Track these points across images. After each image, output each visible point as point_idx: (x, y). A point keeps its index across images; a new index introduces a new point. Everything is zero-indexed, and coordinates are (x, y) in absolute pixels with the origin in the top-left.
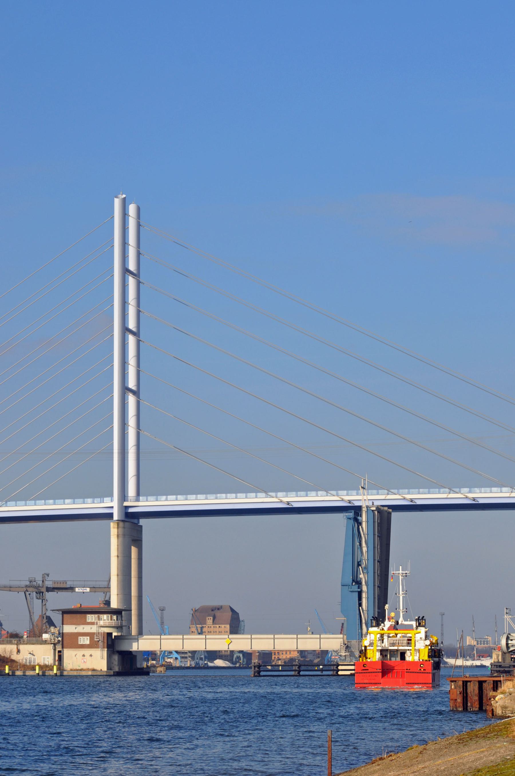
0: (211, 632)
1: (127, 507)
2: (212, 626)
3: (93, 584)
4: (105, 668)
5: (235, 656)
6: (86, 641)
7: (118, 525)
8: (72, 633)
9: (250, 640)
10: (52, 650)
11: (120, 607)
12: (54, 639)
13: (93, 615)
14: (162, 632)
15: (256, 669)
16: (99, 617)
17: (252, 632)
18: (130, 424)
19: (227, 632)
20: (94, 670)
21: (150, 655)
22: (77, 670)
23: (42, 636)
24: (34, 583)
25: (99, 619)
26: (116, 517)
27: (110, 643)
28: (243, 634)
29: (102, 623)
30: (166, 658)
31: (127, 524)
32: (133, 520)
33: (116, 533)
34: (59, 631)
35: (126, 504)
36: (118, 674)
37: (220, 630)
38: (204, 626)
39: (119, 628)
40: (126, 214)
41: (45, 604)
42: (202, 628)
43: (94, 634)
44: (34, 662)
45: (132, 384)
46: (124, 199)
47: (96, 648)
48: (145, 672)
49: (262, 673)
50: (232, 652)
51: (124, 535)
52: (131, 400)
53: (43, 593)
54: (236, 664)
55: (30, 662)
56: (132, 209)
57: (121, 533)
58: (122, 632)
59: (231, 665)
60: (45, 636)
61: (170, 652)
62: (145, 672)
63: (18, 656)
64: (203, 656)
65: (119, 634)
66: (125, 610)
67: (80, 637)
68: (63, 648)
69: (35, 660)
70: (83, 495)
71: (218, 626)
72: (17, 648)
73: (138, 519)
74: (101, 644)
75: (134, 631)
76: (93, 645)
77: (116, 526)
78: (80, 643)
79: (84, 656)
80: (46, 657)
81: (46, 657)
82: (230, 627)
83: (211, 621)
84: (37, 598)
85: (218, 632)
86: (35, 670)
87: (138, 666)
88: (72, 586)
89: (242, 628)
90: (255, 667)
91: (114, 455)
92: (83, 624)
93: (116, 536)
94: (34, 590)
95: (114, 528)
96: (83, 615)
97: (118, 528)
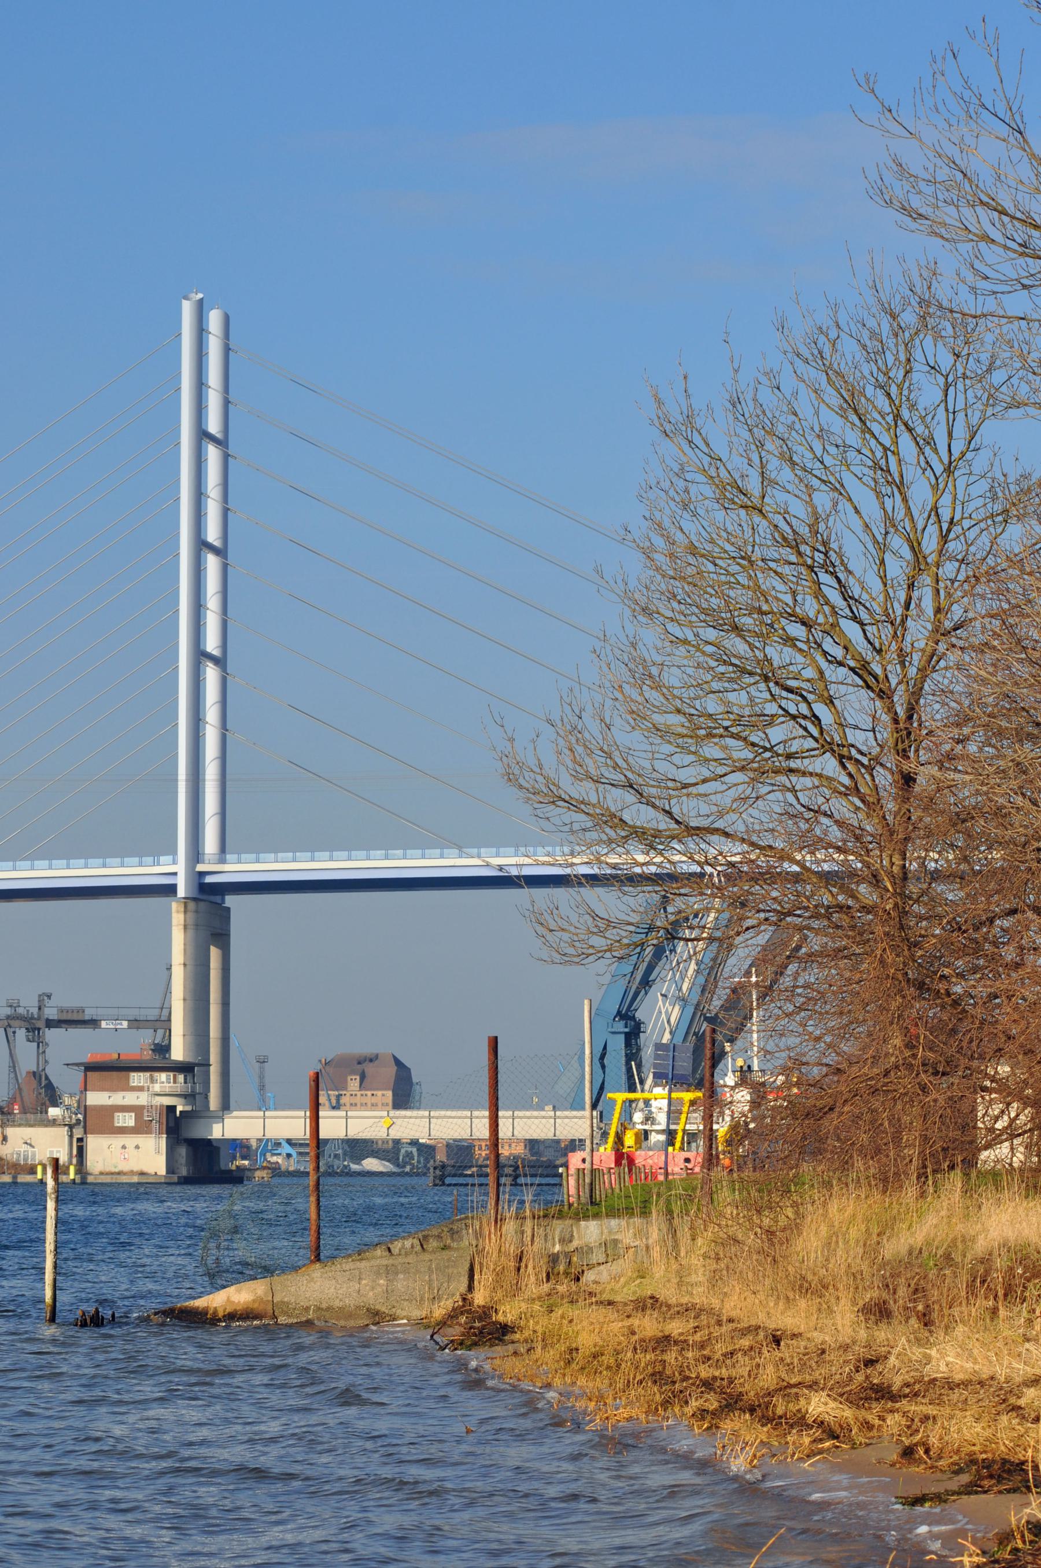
0: (356, 1105)
1: (202, 874)
2: (359, 1093)
3: (134, 1013)
4: (162, 1171)
5: (403, 1151)
6: (127, 1120)
7: (186, 907)
8: (102, 1106)
9: (552, 1121)
10: (67, 1138)
11: (190, 1059)
12: (70, 1117)
13: (141, 1074)
14: (262, 1104)
15: (438, 1172)
16: (152, 1077)
17: (431, 1107)
18: (207, 719)
19: (387, 1105)
20: (142, 1174)
21: (240, 1146)
22: (112, 1174)
23: (47, 1112)
24: (20, 1010)
25: (153, 1081)
26: (181, 892)
27: (172, 1124)
28: (419, 1109)
29: (157, 1088)
30: (268, 1155)
31: (202, 904)
32: (213, 898)
33: (182, 922)
34: (79, 1102)
35: (200, 868)
36: (186, 1181)
37: (374, 1100)
38: (343, 1093)
39: (186, 1097)
40: (203, 330)
41: (44, 1052)
42: (339, 1097)
43: (142, 1107)
44: (33, 1159)
45: (212, 644)
46: (201, 302)
47: (147, 1133)
48: (236, 1178)
49: (448, 1180)
50: (397, 1142)
51: (197, 925)
52: (211, 674)
53: (39, 1029)
54: (404, 1167)
55: (26, 1159)
56: (214, 320)
57: (190, 921)
58: (193, 1104)
59: (395, 1169)
60: (53, 1112)
61: (278, 1144)
62: (236, 1178)
63: (4, 1147)
64: (340, 1152)
65: (189, 1108)
66: (199, 1065)
67: (116, 1114)
68: (85, 1133)
69: (34, 1154)
70: (122, 851)
71: (369, 1093)
72: (2, 1133)
73: (223, 895)
74: (155, 1125)
75: (214, 1101)
76: (141, 1128)
77: (183, 909)
78: (117, 1125)
79: (124, 1147)
80: (55, 1150)
81: (55, 1150)
82: (394, 1095)
83: (357, 1084)
84: (29, 1040)
85: (369, 1105)
86: (35, 1173)
87: (223, 1167)
88: (95, 1018)
89: (417, 1098)
90: (435, 1168)
91: (179, 783)
92: (123, 1090)
93: (182, 927)
94: (23, 1023)
95: (178, 912)
96: (124, 1073)
97: (185, 912)
